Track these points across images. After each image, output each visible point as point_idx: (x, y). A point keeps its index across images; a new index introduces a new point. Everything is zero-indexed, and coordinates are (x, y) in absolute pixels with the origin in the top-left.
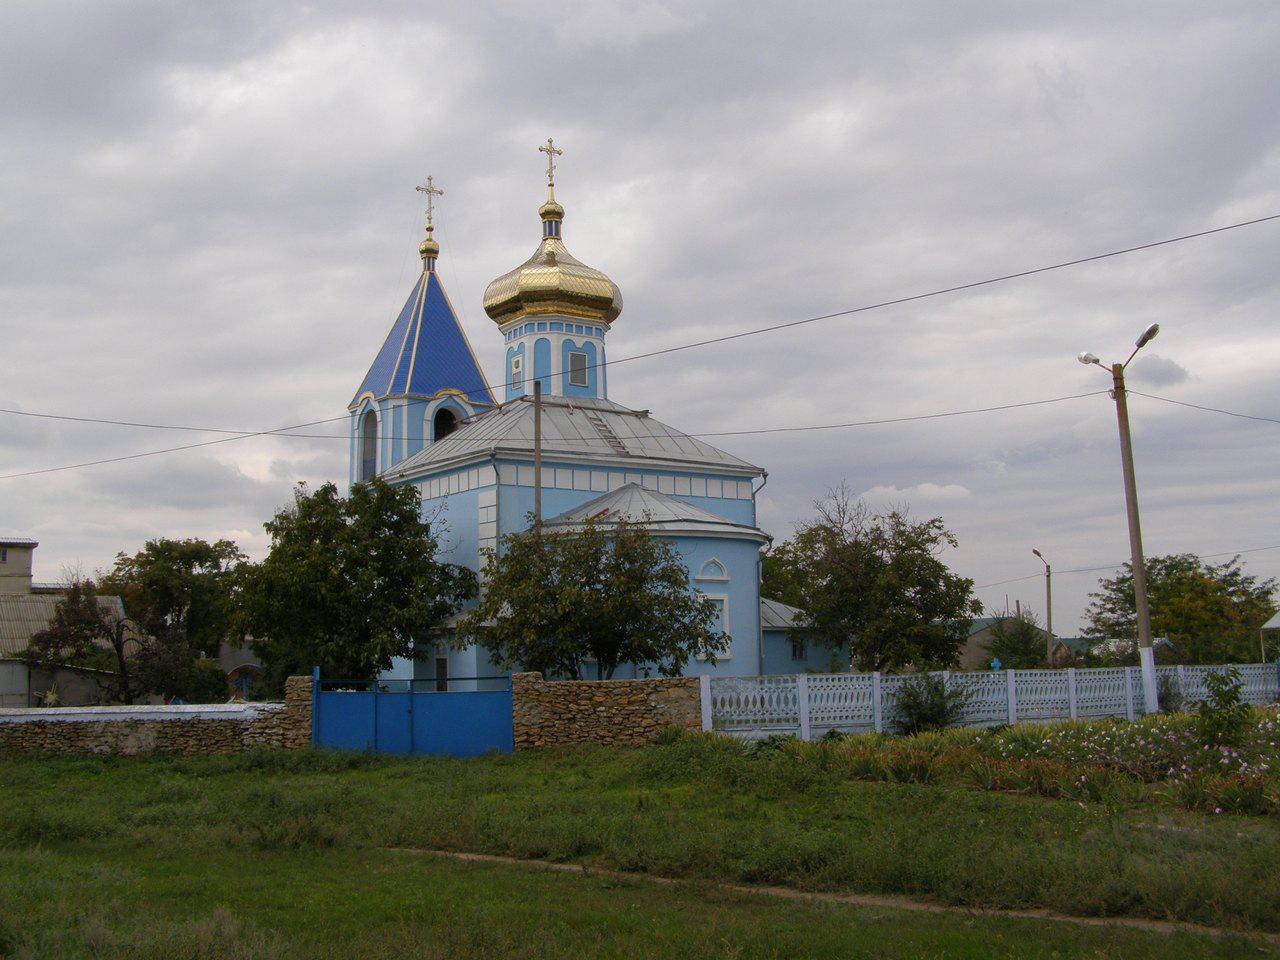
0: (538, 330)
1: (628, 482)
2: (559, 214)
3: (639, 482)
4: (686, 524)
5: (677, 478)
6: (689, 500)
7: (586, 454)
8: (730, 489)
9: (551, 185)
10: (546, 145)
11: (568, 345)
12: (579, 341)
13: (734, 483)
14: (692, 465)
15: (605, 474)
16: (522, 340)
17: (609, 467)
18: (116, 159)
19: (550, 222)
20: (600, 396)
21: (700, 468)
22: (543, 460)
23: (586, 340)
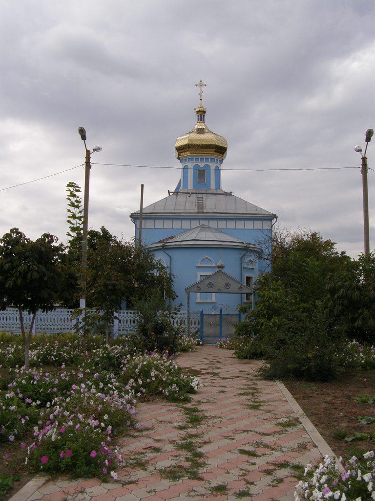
0: (205, 161)
1: (201, 224)
2: (204, 112)
3: (207, 224)
4: (215, 242)
5: (210, 221)
6: (218, 230)
7: (179, 213)
8: (258, 225)
9: (201, 100)
10: (198, 83)
11: (196, 168)
12: (202, 165)
13: (171, 221)
14: (175, 214)
15: (180, 221)
16: (187, 164)
17: (253, 219)
18: (313, 103)
19: (201, 115)
20: (213, 186)
21: (234, 216)
22: (143, 217)
23: (205, 164)
